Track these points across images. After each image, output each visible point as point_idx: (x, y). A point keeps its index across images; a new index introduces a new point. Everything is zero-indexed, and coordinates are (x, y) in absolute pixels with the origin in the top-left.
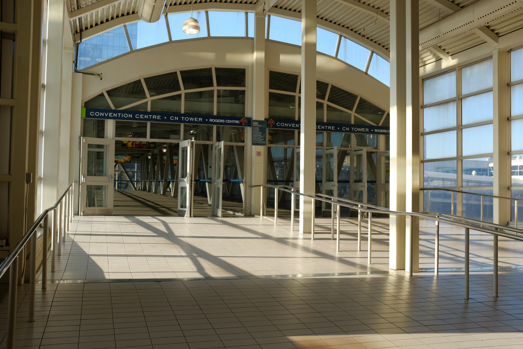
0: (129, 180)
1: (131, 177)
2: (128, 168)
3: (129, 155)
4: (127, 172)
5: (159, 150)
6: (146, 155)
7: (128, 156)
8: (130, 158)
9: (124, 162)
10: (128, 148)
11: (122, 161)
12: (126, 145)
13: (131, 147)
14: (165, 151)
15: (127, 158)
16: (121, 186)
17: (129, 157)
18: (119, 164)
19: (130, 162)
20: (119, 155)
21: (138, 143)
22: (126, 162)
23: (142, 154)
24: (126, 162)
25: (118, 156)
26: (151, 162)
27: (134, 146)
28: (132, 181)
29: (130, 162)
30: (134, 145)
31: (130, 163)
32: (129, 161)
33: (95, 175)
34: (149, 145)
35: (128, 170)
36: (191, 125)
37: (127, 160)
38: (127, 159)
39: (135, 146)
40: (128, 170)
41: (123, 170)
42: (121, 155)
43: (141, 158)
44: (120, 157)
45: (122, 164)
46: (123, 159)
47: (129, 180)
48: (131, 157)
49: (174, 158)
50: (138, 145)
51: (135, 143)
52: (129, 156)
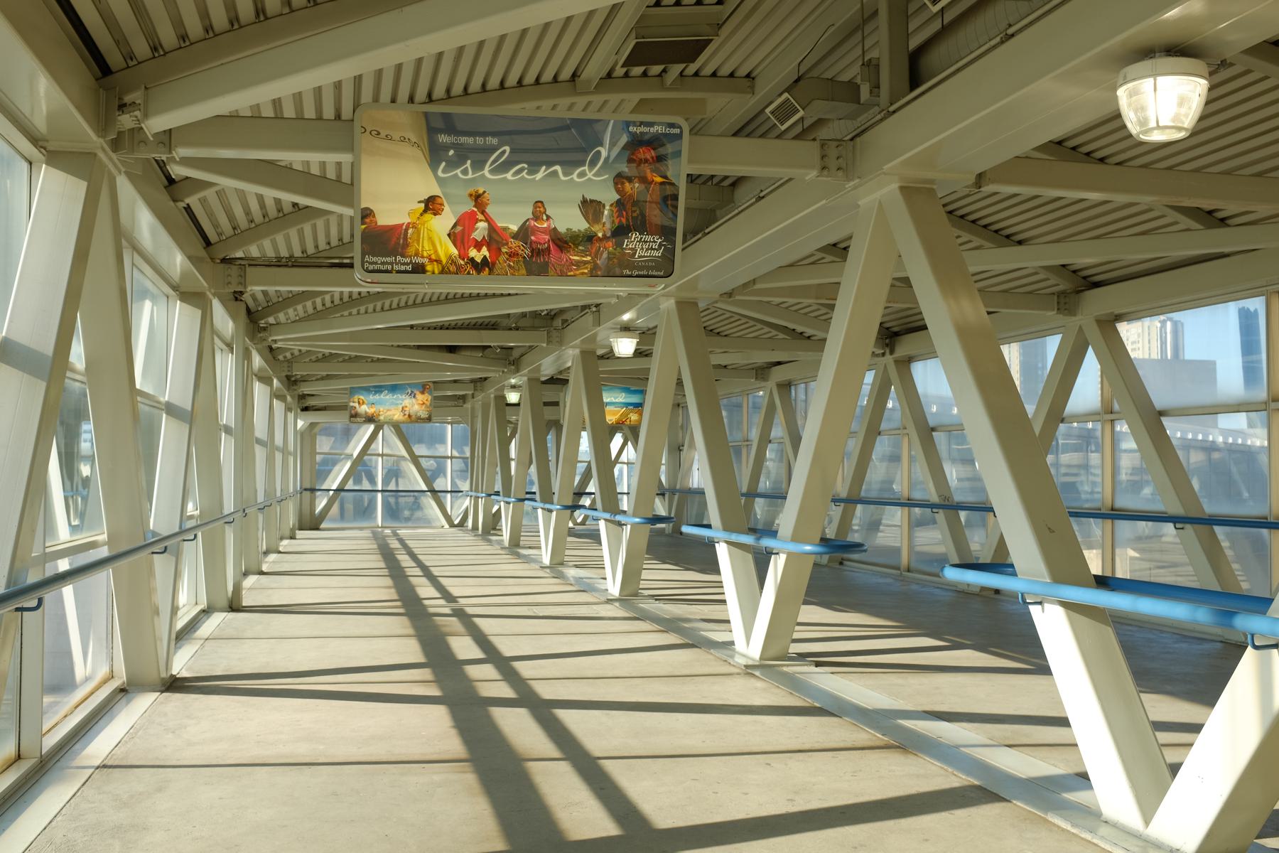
0: (424, 488)
1: (429, 474)
2: (420, 441)
3: (424, 388)
4: (415, 460)
5: (583, 352)
6: (492, 390)
7: (420, 397)
8: (428, 403)
9: (403, 422)
10: (419, 269)
11: (397, 416)
12: (406, 245)
13: (452, 261)
14: (513, 397)
15: (416, 404)
16: (397, 503)
17: (426, 398)
18: (386, 427)
19: (429, 419)
20: (381, 392)
21: (514, 228)
22: (412, 422)
23: (479, 383)
24: (413, 419)
25: (377, 397)
26: (524, 419)
27: (473, 253)
28: (434, 492)
29: (429, 419)
30: (478, 246)
31: (428, 425)
32: (424, 414)
33: (832, 307)
34: (610, 245)
35: (420, 450)
36: (621, 291)
37: (418, 414)
38: (416, 407)
39: (485, 251)
40: (420, 450)
41: (404, 452)
42: (394, 389)
43: (468, 406)
44: (387, 397)
45: (397, 427)
46: (401, 407)
47: (424, 488)
48: (436, 398)
49: (606, 400)
50: (514, 244)
51: (482, 225)
52: (423, 393)
